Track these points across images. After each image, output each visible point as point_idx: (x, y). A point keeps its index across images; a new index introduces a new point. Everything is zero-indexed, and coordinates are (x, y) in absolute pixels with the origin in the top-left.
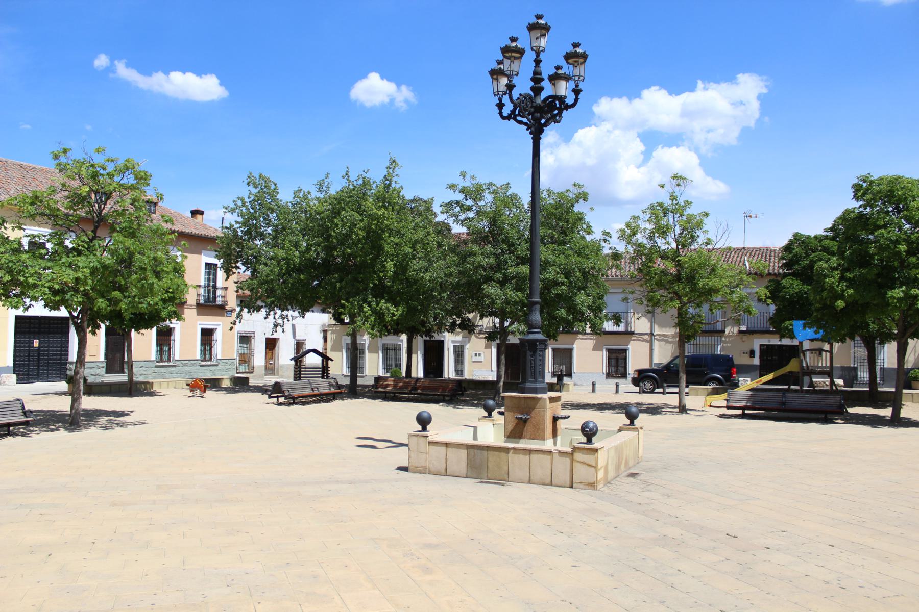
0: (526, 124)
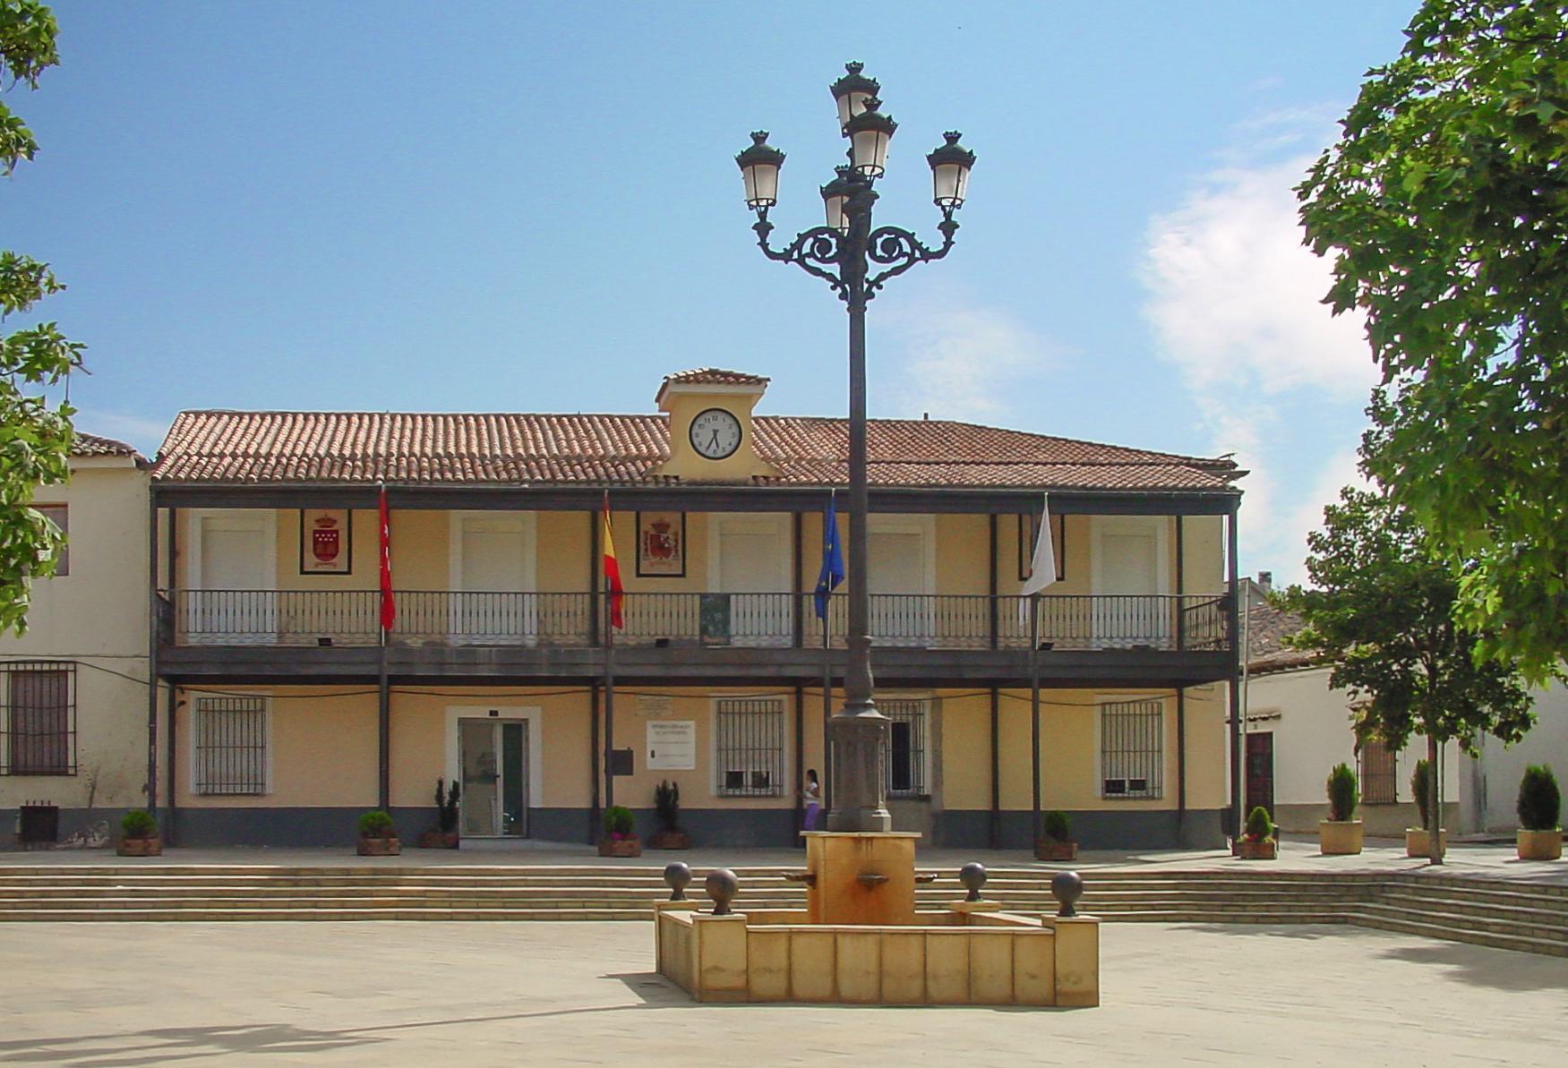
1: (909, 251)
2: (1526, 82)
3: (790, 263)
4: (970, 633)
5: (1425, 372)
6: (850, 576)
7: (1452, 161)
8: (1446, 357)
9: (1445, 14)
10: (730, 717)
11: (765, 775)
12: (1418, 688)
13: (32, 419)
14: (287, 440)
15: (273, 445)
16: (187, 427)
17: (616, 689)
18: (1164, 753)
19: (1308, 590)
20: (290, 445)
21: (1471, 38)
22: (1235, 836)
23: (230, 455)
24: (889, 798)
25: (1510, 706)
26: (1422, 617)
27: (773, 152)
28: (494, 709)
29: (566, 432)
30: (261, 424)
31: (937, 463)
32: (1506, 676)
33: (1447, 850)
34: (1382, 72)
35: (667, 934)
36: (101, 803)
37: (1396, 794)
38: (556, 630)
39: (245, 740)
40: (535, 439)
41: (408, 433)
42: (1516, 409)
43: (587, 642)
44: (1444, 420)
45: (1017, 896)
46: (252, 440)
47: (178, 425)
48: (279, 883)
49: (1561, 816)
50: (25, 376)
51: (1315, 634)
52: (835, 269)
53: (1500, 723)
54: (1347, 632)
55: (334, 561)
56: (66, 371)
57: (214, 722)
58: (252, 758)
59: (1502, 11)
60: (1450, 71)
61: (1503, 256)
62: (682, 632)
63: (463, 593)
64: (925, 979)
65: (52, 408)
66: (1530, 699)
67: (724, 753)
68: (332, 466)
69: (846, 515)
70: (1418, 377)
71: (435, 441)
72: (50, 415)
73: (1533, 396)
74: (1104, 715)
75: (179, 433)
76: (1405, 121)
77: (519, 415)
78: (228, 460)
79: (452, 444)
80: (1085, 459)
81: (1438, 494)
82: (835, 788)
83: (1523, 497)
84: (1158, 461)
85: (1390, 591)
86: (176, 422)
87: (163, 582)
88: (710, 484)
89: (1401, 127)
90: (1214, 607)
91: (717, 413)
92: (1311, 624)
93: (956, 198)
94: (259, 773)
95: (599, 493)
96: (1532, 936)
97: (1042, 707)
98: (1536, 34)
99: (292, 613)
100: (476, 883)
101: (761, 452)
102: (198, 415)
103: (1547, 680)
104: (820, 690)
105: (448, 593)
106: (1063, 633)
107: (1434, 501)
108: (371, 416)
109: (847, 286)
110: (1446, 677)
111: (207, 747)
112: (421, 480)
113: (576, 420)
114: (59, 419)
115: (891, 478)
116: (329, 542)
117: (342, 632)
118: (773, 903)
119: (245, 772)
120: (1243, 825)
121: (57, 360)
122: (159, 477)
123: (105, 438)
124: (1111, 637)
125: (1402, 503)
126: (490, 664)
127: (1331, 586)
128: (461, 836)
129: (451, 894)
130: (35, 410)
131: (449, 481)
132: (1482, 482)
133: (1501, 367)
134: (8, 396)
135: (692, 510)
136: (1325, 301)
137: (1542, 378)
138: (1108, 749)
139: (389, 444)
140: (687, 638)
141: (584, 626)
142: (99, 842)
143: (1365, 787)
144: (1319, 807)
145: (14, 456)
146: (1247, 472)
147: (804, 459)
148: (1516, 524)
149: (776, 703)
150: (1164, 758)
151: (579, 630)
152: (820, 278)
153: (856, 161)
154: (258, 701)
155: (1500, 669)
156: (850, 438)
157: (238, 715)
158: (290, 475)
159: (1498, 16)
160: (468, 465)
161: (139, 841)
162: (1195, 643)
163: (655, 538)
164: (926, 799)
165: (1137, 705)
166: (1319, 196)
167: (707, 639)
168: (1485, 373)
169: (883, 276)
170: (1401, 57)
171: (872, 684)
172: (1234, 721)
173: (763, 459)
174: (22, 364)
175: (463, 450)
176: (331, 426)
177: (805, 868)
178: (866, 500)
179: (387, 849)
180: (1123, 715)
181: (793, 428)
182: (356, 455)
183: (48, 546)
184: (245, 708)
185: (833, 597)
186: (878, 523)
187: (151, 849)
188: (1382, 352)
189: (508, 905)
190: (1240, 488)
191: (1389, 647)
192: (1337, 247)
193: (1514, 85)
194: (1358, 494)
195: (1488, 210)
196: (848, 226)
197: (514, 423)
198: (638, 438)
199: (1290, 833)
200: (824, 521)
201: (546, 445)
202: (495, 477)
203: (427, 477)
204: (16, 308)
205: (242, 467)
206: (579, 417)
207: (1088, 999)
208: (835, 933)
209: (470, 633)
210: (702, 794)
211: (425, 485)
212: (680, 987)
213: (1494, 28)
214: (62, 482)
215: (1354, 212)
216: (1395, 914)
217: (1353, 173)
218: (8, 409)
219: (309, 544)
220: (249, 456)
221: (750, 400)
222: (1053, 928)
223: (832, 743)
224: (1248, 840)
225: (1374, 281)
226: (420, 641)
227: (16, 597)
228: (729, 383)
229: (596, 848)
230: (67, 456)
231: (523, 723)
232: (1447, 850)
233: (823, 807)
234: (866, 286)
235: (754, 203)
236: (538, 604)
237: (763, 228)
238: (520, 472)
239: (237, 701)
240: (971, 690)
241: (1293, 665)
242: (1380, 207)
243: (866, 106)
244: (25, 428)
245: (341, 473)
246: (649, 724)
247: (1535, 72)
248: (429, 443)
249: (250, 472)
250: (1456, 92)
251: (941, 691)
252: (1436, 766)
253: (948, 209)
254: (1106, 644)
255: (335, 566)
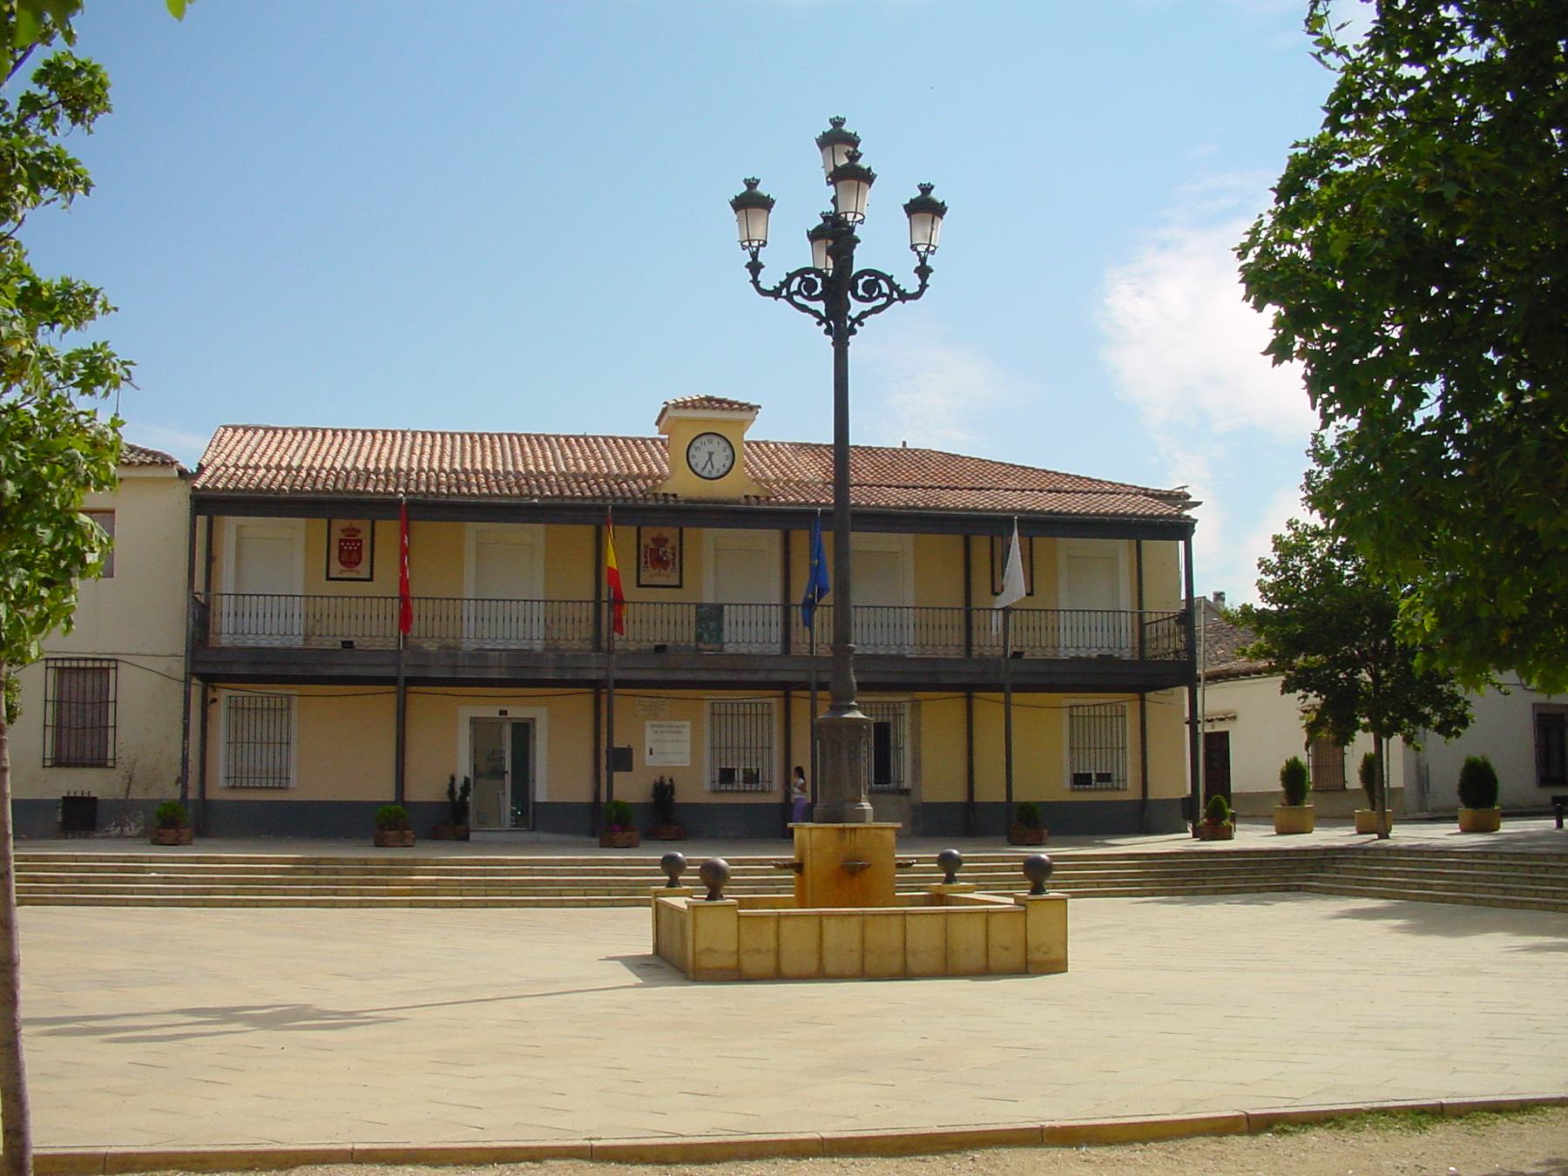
0: (816, 313)
1: (888, 292)
2: (1431, 161)
3: (780, 300)
4: (948, 644)
5: (1358, 421)
6: (835, 590)
7: (1372, 232)
8: (1376, 408)
9: (1357, 93)
10: (723, 718)
11: (755, 772)
12: (1363, 693)
13: (85, 430)
14: (317, 454)
15: (304, 458)
16: (225, 440)
17: (616, 691)
18: (1128, 750)
19: (1259, 608)
20: (320, 459)
21: (1380, 117)
22: (1195, 819)
23: (265, 467)
24: (871, 792)
25: (1449, 708)
26: (1365, 633)
27: (763, 197)
28: (504, 709)
29: (573, 452)
30: (293, 439)
31: (915, 488)
32: (1445, 684)
33: (1393, 826)
34: (1306, 145)
35: (663, 920)
36: (137, 794)
37: (1345, 782)
38: (562, 635)
39: (271, 736)
40: (544, 457)
41: (427, 449)
42: (1443, 457)
43: (591, 647)
44: (1378, 464)
45: (991, 878)
46: (285, 453)
47: (218, 438)
48: (300, 872)
49: (1499, 797)
50: (80, 389)
51: (1266, 646)
52: (820, 306)
53: (1441, 722)
54: (1296, 645)
55: (358, 568)
56: (117, 386)
57: (243, 719)
58: (277, 754)
59: (1405, 93)
60: (1365, 148)
61: (1422, 320)
62: (679, 639)
63: (476, 600)
64: (905, 954)
65: (103, 419)
66: (1467, 703)
67: (717, 751)
68: (358, 478)
69: (831, 534)
70: (1353, 424)
71: (452, 457)
72: (101, 427)
73: (1457, 447)
74: (1071, 716)
75: (218, 446)
76: (1329, 192)
77: (530, 435)
78: (262, 472)
79: (468, 460)
80: (1051, 487)
81: (1376, 528)
82: (821, 783)
83: (1453, 533)
84: (1118, 490)
85: (1336, 611)
86: (216, 434)
87: (199, 585)
88: (706, 502)
89: (1325, 198)
90: (1172, 621)
91: (712, 437)
92: (1263, 637)
93: (930, 245)
94: (284, 767)
95: (603, 509)
96: (1474, 892)
97: (1014, 710)
98: (1436, 117)
99: (318, 617)
100: (484, 873)
101: (753, 474)
102: (235, 429)
103: (1482, 687)
104: (807, 693)
105: (462, 600)
106: (1034, 643)
107: (1372, 533)
108: (394, 433)
109: (831, 322)
110: (1389, 684)
111: (236, 742)
112: (439, 493)
113: (582, 440)
114: (109, 431)
115: (873, 500)
116: (353, 550)
117: (364, 635)
118: (762, 889)
119: (271, 766)
120: (1202, 811)
121: (108, 376)
122: (199, 486)
123: (151, 449)
124: (1078, 647)
125: (1343, 536)
126: (500, 667)
127: (1280, 605)
128: (472, 828)
129: (460, 883)
130: (88, 421)
131: (465, 495)
132: (1415, 519)
133: (1428, 420)
134: (64, 408)
135: (689, 526)
136: (1265, 353)
137: (1464, 431)
138: (1076, 746)
139: (410, 460)
140: (683, 644)
141: (588, 631)
142: (135, 831)
143: (1316, 776)
144: (1274, 794)
145: (67, 464)
146: (1200, 503)
147: (792, 481)
148: (1448, 556)
149: (766, 706)
150: (1128, 754)
151: (584, 636)
152: (807, 314)
153: (840, 207)
154: (285, 699)
155: (1438, 678)
156: (835, 462)
157: (266, 712)
158: (319, 486)
159: (1403, 98)
160: (483, 480)
161: (172, 831)
162: (1155, 653)
163: (654, 551)
164: (906, 792)
165: (1103, 708)
166: (1257, 256)
167: (702, 646)
168: (1413, 424)
169: (864, 314)
170: (1321, 132)
171: (856, 688)
172: (1193, 722)
173: (754, 480)
174: (77, 379)
175: (479, 466)
176: (358, 442)
177: (792, 857)
178: (850, 520)
179: (402, 841)
180: (1089, 716)
181: (782, 452)
182: (380, 469)
183: (96, 549)
184: (272, 706)
185: (819, 608)
186: (860, 541)
187: (182, 838)
188: (1319, 401)
189: (514, 893)
190: (1193, 517)
191: (1335, 659)
192: (1274, 305)
193: (1420, 164)
194: (1303, 526)
195: (1406, 278)
196: (832, 267)
197: (526, 442)
198: (639, 458)
199: (1246, 817)
200: (810, 539)
201: (554, 463)
202: (508, 492)
203: (445, 491)
204: (73, 328)
205: (275, 478)
206: (586, 438)
207: (1057, 965)
208: (821, 915)
209: (482, 638)
210: (696, 789)
211: (443, 499)
212: (676, 967)
213: (1400, 109)
214: (111, 489)
215: (1288, 274)
216: (1345, 881)
217: (1285, 237)
218: (64, 420)
219: (335, 552)
220: (281, 468)
221: (743, 425)
222: (1025, 905)
223: (818, 742)
224: (1206, 824)
225: (1309, 337)
226: (436, 645)
227: (65, 597)
228: (724, 409)
229: (598, 840)
230: (116, 465)
231: (531, 722)
232: (1393, 826)
233: (810, 801)
234: (849, 322)
235: (747, 244)
236: (546, 611)
237: (755, 267)
238: (530, 487)
239: (265, 699)
240: (947, 694)
241: (1247, 674)
242: (1311, 270)
243: (849, 158)
244: (78, 438)
245: (365, 486)
246: (648, 723)
247: (1438, 153)
248: (447, 459)
249: (283, 483)
250: (1371, 168)
251: (919, 695)
252: (1382, 757)
253: (923, 254)
254: (1072, 653)
255: (358, 573)
